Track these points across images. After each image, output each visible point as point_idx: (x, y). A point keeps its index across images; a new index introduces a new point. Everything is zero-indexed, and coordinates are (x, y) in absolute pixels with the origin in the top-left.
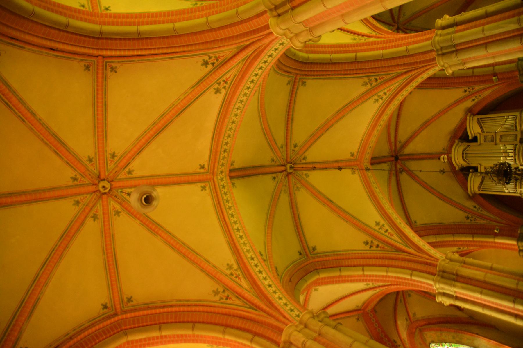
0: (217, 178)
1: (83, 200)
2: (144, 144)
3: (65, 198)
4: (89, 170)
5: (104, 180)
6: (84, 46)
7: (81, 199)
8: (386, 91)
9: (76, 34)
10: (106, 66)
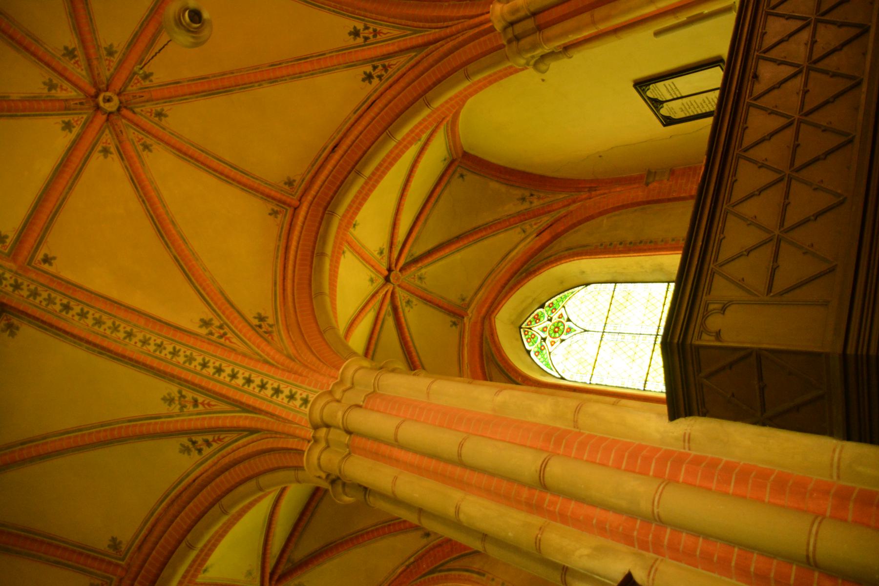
0: (11, 271)
1: (107, 62)
2: (145, 194)
3: (129, 45)
4: (148, 101)
5: (119, 110)
6: (320, 192)
7: (113, 61)
8: (200, 400)
9: (342, 182)
10: (283, 207)
